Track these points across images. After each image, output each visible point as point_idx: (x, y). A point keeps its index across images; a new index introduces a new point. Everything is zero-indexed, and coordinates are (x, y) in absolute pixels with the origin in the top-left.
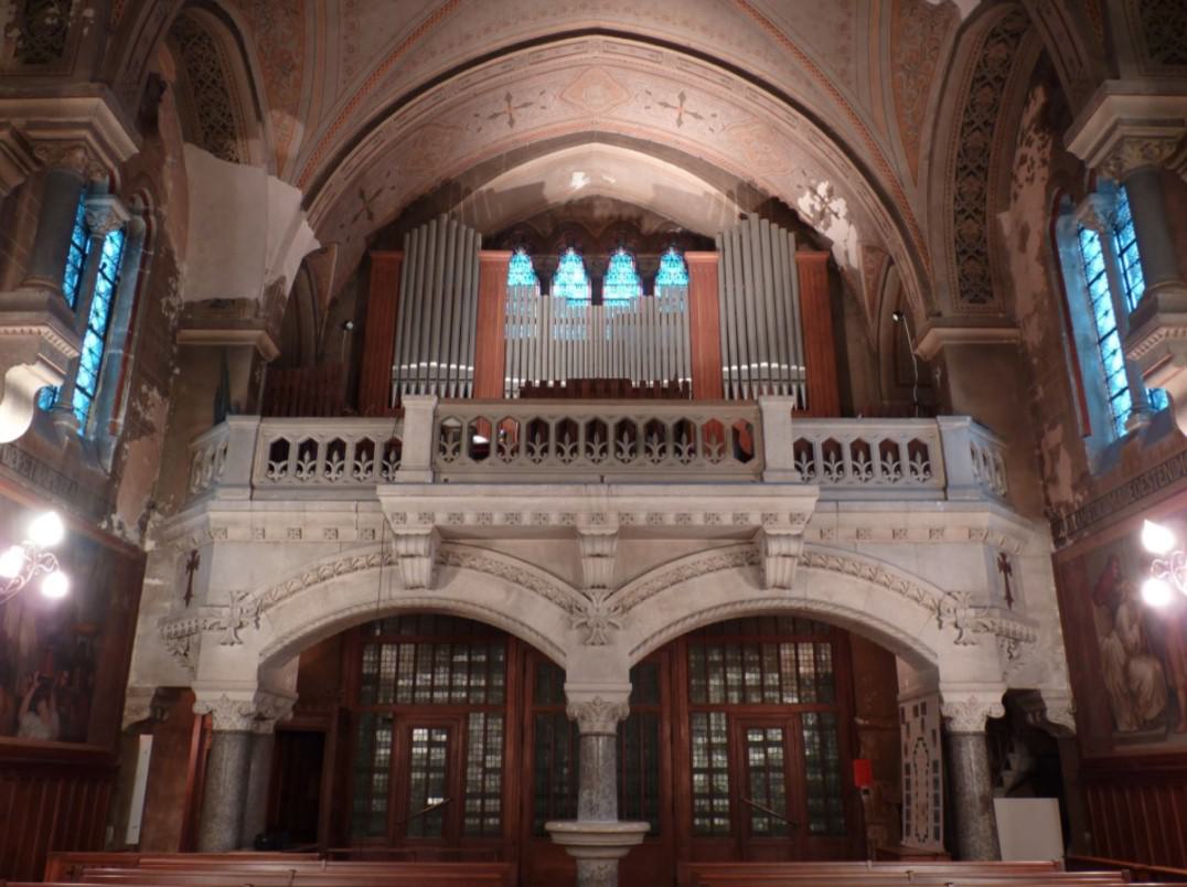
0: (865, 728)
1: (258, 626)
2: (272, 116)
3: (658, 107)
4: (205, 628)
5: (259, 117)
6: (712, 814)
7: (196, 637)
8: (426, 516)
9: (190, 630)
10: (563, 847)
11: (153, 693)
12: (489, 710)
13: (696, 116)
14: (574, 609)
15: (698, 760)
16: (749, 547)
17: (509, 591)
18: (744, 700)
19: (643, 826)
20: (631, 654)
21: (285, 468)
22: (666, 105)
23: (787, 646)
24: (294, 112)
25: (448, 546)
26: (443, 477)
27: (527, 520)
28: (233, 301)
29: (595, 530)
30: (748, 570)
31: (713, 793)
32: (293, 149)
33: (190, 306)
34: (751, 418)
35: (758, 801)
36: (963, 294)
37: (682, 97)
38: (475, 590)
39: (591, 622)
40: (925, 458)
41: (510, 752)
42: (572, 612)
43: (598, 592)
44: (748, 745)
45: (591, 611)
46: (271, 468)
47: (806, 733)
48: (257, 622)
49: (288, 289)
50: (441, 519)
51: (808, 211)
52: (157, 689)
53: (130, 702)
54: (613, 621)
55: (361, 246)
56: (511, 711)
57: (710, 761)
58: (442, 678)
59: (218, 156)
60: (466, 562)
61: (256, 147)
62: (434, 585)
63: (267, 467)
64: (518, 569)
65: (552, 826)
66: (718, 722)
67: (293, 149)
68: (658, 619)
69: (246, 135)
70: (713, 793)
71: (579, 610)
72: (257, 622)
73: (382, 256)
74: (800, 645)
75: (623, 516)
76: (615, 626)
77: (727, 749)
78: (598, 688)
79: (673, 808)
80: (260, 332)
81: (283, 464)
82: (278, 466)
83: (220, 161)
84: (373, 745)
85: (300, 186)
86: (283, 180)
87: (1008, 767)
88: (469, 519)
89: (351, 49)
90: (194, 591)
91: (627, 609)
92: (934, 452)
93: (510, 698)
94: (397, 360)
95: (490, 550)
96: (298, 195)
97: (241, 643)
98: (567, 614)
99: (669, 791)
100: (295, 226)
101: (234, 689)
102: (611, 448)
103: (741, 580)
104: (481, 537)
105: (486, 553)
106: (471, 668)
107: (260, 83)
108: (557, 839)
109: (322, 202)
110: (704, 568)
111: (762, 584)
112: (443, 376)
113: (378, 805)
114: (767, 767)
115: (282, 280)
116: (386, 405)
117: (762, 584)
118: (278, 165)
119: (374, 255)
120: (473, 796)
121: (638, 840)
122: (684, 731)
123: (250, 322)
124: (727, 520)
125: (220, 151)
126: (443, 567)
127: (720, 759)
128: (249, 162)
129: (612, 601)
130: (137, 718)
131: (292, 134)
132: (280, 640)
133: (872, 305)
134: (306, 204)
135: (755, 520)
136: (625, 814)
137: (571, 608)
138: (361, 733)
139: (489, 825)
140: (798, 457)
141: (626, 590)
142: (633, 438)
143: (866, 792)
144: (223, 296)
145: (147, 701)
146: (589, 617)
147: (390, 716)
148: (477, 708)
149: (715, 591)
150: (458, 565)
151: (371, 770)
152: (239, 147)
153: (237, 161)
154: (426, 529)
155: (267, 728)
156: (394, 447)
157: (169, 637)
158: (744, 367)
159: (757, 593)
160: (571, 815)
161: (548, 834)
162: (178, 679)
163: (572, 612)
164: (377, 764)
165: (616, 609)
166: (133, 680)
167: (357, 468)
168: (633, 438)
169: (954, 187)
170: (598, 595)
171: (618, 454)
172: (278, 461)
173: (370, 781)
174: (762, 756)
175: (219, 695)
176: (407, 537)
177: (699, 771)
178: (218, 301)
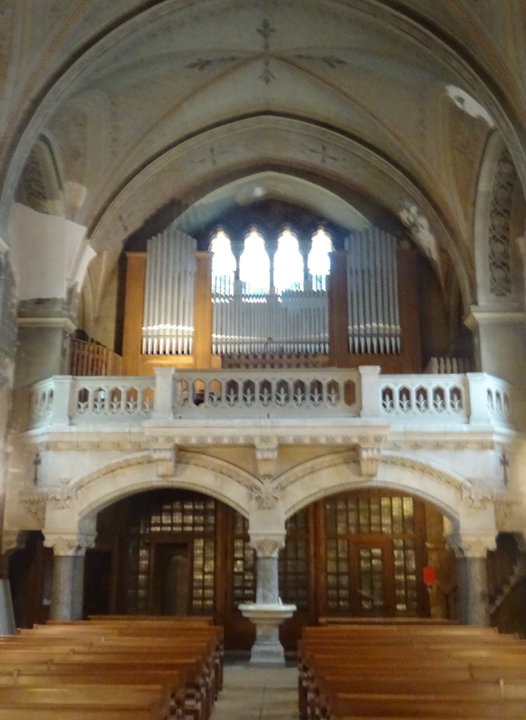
0: (432, 549)
1: (77, 498)
2: (68, 185)
3: (309, 152)
4: (47, 499)
5: (61, 187)
6: (338, 599)
7: (42, 504)
8: (169, 439)
9: (39, 499)
10: (247, 619)
11: (17, 533)
12: (203, 535)
13: (334, 159)
14: (254, 489)
15: (331, 567)
16: (351, 453)
17: (216, 478)
18: (359, 532)
19: (292, 608)
20: (286, 513)
21: (87, 407)
22: (314, 151)
23: (385, 498)
24: (81, 181)
25: (183, 453)
26: (179, 415)
27: (226, 441)
28: (49, 300)
29: (265, 446)
30: (353, 466)
31: (338, 587)
32: (81, 203)
33: (23, 303)
34: (354, 379)
35: (365, 593)
36: (492, 291)
37: (324, 148)
38: (198, 477)
39: (263, 496)
40: (459, 398)
41: (219, 562)
42: (252, 490)
43: (267, 480)
44: (360, 558)
45: (263, 490)
46: (79, 406)
47: (396, 552)
48: (76, 496)
49: (79, 289)
50: (177, 441)
51: (406, 220)
52: (19, 531)
53: (5, 539)
54: (274, 495)
55: (120, 247)
56: (219, 538)
57: (338, 568)
58: (177, 518)
59: (35, 210)
60: (193, 461)
61: (59, 205)
62: (174, 475)
63: (76, 406)
64: (221, 466)
65: (242, 607)
66: (342, 544)
67: (81, 203)
68: (300, 494)
69: (53, 197)
70: (338, 587)
71: (256, 489)
72: (76, 496)
73: (132, 256)
74: (393, 499)
75: (279, 438)
76: (276, 499)
77: (348, 560)
78: (267, 530)
79: (316, 596)
80: (65, 319)
81: (85, 403)
82: (83, 405)
83: (37, 213)
84: (138, 559)
85: (85, 224)
86: (75, 222)
87: (512, 573)
88: (194, 441)
89: (114, 140)
90: (39, 477)
91: (283, 488)
92: (463, 395)
93: (219, 530)
94: (145, 323)
95: (205, 454)
96: (83, 230)
97: (68, 507)
98: (249, 491)
99: (313, 585)
100: (83, 249)
101: (66, 534)
102: (274, 398)
103: (348, 471)
104: (201, 450)
105: (204, 457)
106: (194, 512)
107: (61, 165)
108: (245, 615)
109: (99, 232)
110: (327, 464)
111: (360, 474)
112: (174, 333)
113: (142, 593)
114: (372, 570)
115: (76, 285)
116: (139, 352)
117: (360, 474)
118: (72, 213)
119: (131, 255)
120: (198, 588)
121: (290, 615)
122: (322, 550)
123: (60, 312)
124: (339, 441)
125: (36, 207)
126: (179, 464)
127: (344, 567)
128: (55, 214)
129: (275, 483)
130: (9, 548)
131: (80, 194)
132: (90, 505)
133: (446, 282)
134: (89, 235)
135: (355, 440)
136: (286, 600)
137: (252, 488)
138: (131, 551)
139: (207, 605)
140: (384, 398)
141: (283, 478)
142: (287, 391)
143: (431, 587)
144: (44, 296)
145: (14, 538)
146: (262, 493)
147: (147, 541)
148: (199, 536)
149: (331, 479)
150: (187, 463)
151: (137, 573)
152: (48, 204)
153: (47, 213)
154: (170, 446)
155: (82, 553)
156: (149, 393)
157: (26, 502)
158: (362, 326)
159: (358, 479)
160: (253, 599)
161: (240, 612)
162: (33, 526)
163: (252, 490)
164: (140, 569)
165: (277, 488)
166: (6, 526)
167: (128, 406)
168: (287, 391)
169: (489, 223)
170: (267, 481)
171: (278, 401)
172: (83, 402)
173: (137, 579)
174: (369, 565)
175: (57, 537)
176: (160, 450)
177: (331, 574)
178: (40, 299)
